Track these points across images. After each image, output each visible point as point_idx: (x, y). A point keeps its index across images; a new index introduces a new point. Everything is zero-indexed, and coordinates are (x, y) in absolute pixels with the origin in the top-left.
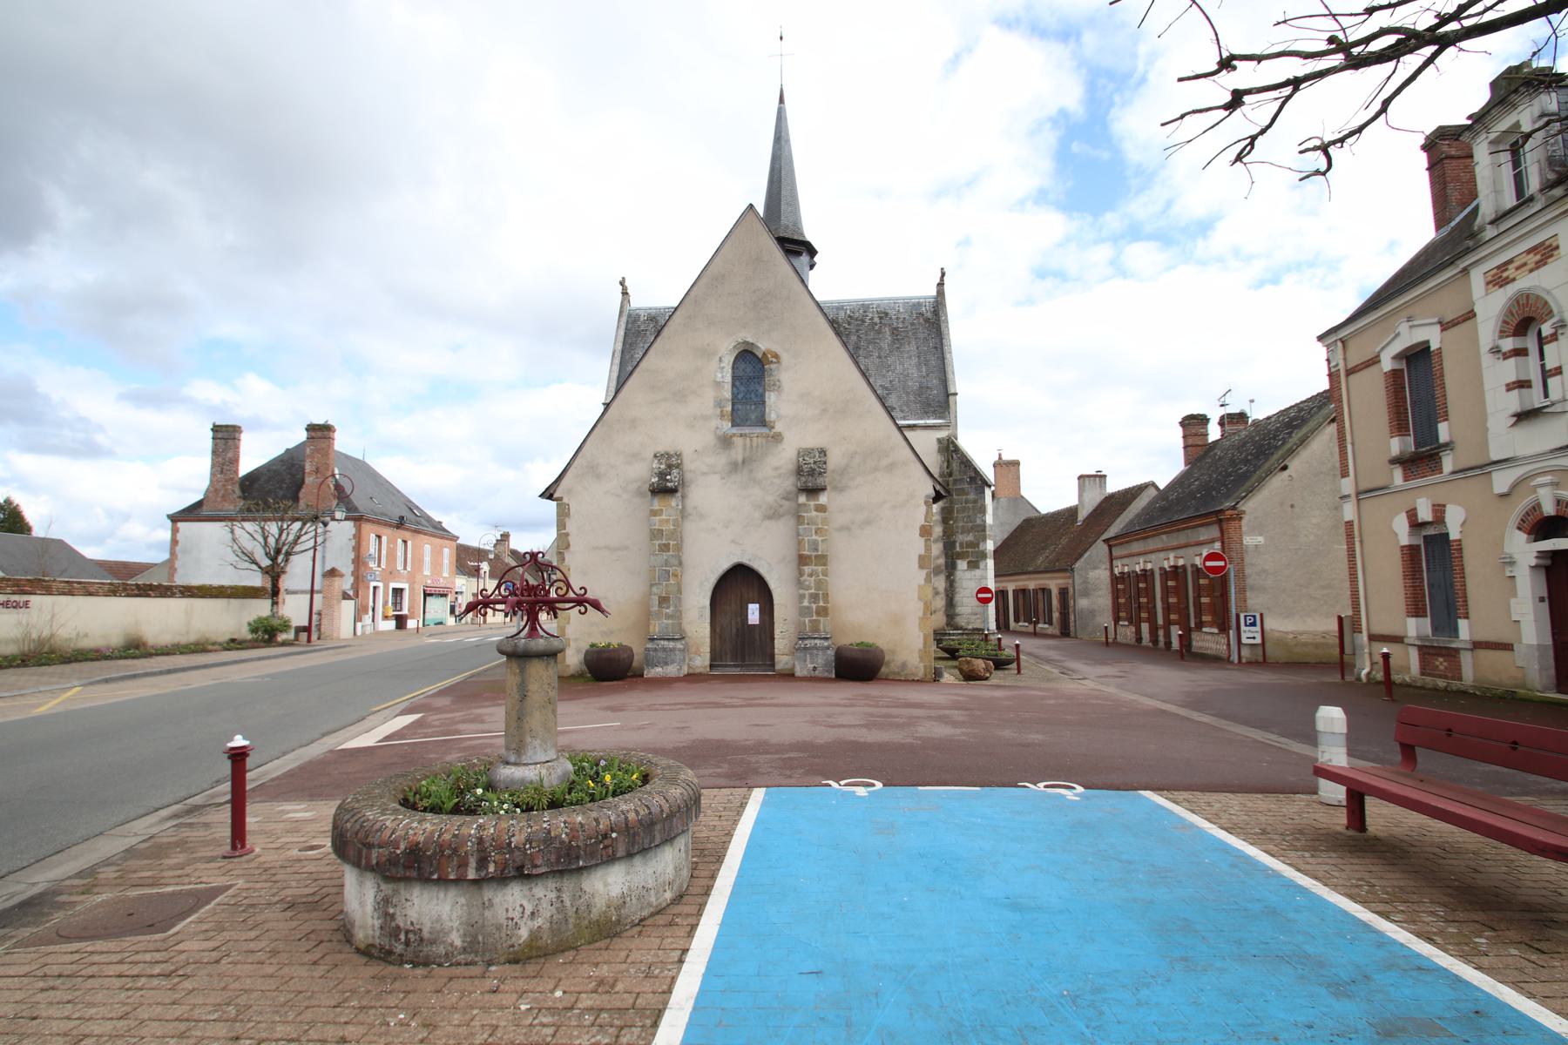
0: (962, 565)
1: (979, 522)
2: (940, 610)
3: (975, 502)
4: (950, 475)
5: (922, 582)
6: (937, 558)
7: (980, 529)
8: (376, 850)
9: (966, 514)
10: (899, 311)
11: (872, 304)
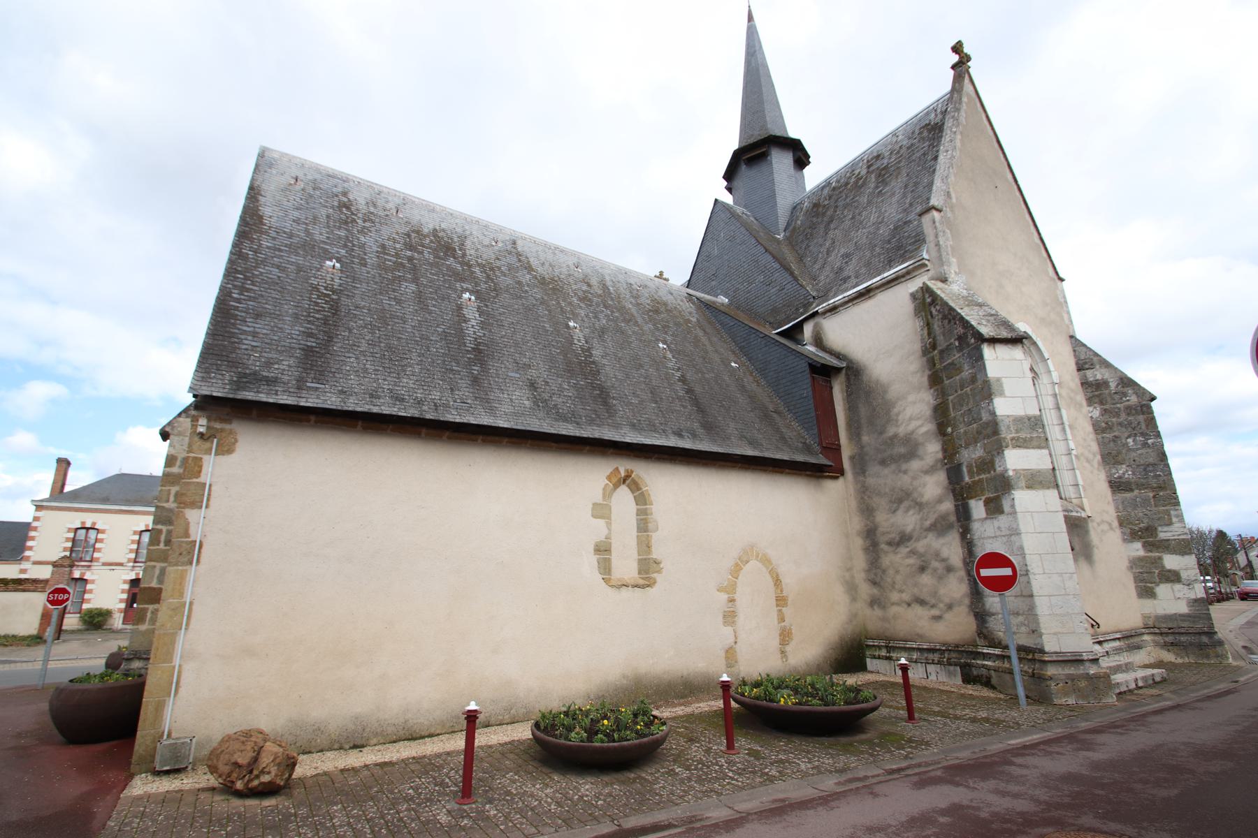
0: (978, 508)
1: (985, 417)
2: (960, 603)
3: (973, 379)
4: (934, 346)
6: (940, 501)
7: (989, 431)
8: (273, 774)
9: (965, 408)
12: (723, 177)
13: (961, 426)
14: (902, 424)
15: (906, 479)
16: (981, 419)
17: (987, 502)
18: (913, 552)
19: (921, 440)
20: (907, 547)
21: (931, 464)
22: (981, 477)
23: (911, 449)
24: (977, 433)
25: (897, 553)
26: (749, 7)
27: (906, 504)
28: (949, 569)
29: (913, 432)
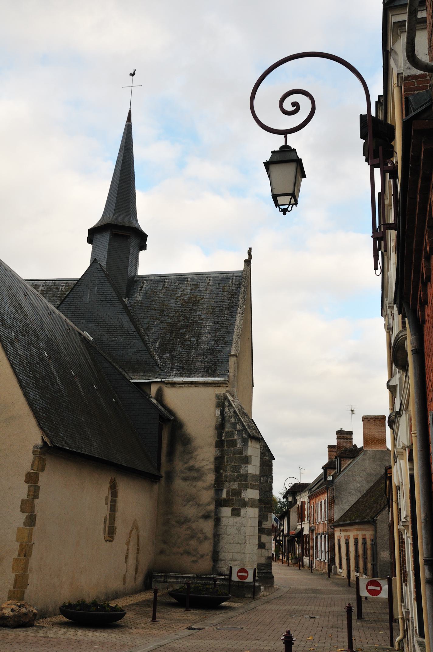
0: (226, 511)
2: (207, 555)
5: (21, 525)
6: (208, 504)
10: (209, 283)
11: (187, 278)
12: (89, 230)
13: (228, 472)
14: (198, 461)
15: (194, 490)
16: (240, 472)
17: (233, 510)
18: (190, 528)
19: (205, 471)
20: (187, 525)
21: (208, 485)
22: (233, 498)
23: (199, 474)
24: (236, 477)
25: (181, 528)
26: (130, 108)
27: (191, 503)
28: (206, 538)
29: (203, 467)
